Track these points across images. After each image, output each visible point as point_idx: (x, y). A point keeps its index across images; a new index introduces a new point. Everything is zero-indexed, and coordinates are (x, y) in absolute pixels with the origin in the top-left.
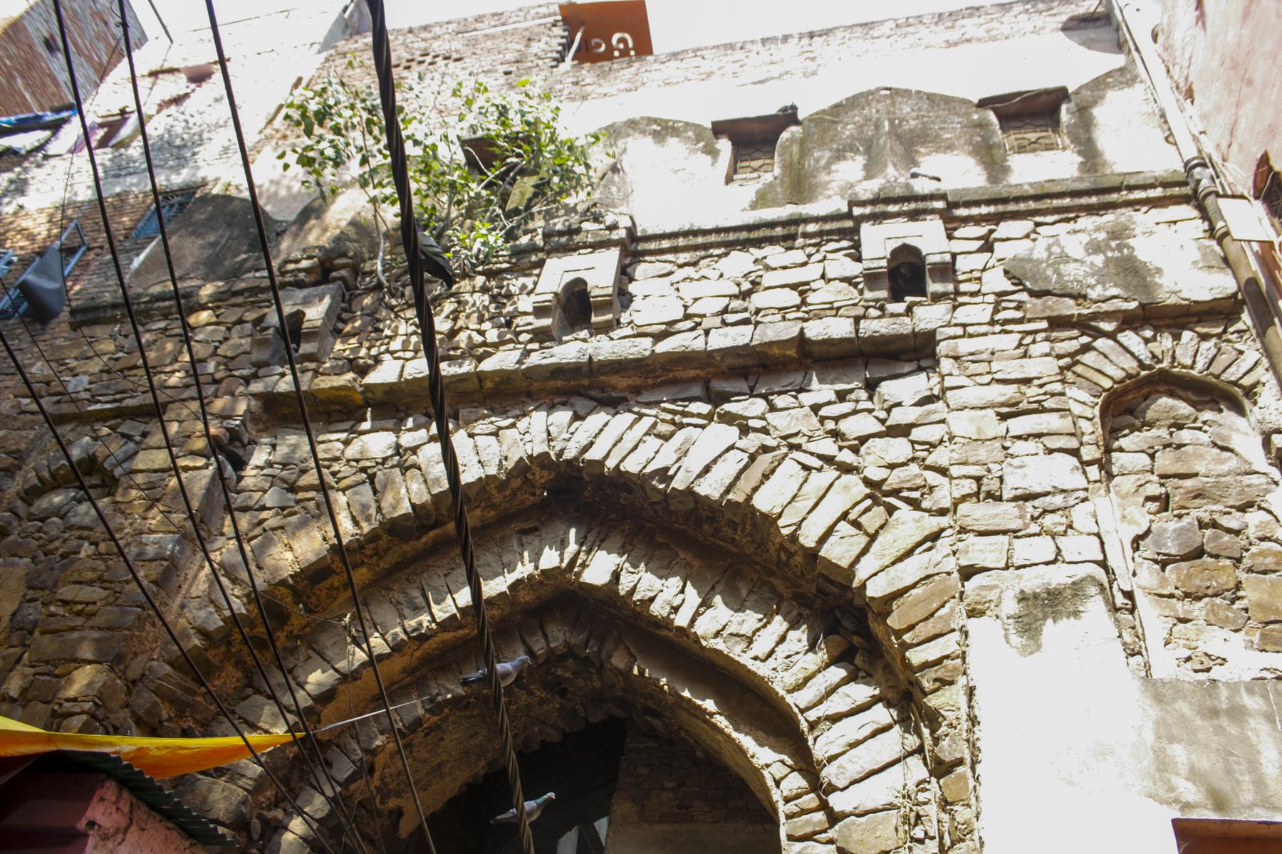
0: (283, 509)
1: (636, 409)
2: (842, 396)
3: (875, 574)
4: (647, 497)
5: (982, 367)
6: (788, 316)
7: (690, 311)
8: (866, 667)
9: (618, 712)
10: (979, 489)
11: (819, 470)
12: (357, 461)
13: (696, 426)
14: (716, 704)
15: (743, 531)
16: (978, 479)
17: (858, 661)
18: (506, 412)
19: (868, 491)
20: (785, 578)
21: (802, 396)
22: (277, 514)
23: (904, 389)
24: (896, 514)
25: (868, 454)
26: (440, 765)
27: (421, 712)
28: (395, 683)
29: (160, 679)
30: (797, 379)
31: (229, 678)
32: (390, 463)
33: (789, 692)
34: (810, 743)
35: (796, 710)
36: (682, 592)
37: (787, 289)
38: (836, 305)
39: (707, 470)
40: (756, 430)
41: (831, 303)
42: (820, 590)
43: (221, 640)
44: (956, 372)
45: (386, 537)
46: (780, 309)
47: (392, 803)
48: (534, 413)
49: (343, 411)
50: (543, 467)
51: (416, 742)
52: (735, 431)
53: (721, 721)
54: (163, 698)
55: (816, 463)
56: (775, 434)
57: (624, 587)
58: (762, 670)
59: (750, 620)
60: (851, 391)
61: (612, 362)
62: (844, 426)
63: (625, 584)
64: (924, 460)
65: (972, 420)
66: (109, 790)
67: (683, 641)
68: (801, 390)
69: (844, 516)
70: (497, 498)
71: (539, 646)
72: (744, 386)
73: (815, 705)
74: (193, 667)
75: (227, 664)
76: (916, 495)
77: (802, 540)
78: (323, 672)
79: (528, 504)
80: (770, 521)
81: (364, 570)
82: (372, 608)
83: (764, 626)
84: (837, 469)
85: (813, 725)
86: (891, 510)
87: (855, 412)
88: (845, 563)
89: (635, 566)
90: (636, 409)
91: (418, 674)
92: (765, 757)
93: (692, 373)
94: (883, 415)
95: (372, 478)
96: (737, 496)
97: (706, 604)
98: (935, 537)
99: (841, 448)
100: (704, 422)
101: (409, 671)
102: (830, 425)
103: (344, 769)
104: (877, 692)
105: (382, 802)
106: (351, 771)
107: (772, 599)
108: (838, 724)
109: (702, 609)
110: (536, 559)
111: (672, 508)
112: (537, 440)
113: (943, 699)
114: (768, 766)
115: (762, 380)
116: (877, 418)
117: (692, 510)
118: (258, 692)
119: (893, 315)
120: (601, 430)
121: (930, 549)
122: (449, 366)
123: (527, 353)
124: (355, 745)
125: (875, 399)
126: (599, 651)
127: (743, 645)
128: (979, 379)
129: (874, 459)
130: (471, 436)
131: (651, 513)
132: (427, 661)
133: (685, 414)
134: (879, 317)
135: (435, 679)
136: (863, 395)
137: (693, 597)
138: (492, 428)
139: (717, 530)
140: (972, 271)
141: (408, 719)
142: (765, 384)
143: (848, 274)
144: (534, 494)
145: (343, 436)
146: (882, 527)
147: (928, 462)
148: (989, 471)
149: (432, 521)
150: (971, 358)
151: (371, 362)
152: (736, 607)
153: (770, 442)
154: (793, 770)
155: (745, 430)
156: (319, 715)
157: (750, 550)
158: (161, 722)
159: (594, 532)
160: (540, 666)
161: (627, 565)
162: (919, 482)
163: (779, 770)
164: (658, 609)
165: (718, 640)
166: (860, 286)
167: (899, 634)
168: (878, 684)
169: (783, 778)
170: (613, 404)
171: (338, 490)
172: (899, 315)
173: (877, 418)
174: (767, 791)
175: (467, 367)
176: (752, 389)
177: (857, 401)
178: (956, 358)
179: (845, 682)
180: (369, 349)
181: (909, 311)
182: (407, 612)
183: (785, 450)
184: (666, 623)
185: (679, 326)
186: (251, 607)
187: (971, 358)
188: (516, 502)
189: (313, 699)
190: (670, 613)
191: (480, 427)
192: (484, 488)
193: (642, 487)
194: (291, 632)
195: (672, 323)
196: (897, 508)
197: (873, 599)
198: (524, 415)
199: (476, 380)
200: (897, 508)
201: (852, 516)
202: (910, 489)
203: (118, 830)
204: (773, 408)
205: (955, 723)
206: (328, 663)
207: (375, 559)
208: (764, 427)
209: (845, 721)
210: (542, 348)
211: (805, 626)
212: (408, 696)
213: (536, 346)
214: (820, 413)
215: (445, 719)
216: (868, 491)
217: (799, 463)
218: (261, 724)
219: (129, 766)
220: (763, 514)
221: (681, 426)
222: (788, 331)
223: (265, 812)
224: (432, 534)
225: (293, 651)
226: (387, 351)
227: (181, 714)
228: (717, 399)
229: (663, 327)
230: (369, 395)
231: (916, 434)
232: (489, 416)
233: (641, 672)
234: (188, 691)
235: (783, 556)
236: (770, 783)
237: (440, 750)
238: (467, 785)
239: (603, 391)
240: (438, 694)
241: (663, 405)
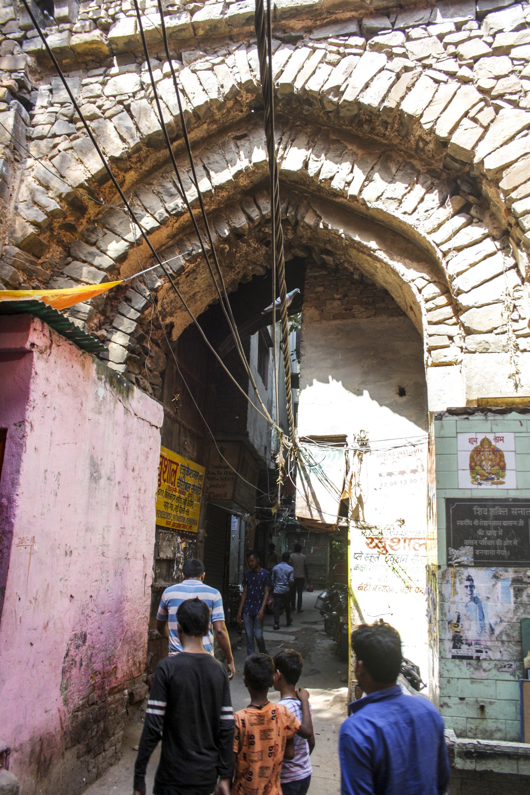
0: (69, 135)
1: (310, 44)
2: (459, 27)
3: (490, 154)
4: (323, 107)
8: (479, 216)
9: (301, 254)
11: (446, 83)
12: (115, 96)
13: (355, 54)
14: (377, 243)
15: (392, 128)
17: (473, 212)
18: (216, 52)
19: (481, 96)
20: (421, 160)
21: (430, 28)
22: (66, 139)
24: (501, 112)
25: (481, 69)
26: (195, 295)
27: (183, 262)
28: (162, 246)
29: (14, 256)
30: (425, 15)
31: (55, 253)
32: (139, 96)
33: (429, 233)
34: (444, 265)
35: (434, 245)
36: (352, 172)
39: (367, 86)
40: (398, 55)
42: (445, 167)
43: (47, 228)
45: (145, 149)
47: (168, 320)
48: (237, 52)
49: (92, 60)
50: (248, 91)
51: (180, 281)
52: (384, 57)
53: (381, 255)
54: (18, 269)
55: (444, 77)
56: (412, 57)
57: (312, 172)
58: (409, 220)
59: (398, 188)
60: (466, 22)
61: (292, 9)
62: (462, 49)
64: (520, 72)
66: (37, 324)
67: (354, 204)
68: (429, 24)
69: (466, 114)
70: (218, 115)
71: (255, 214)
72: (386, 22)
73: (446, 241)
74: (32, 246)
75: (52, 243)
76: (515, 97)
77: (437, 132)
78: (117, 242)
79: (238, 118)
80: (415, 120)
81: (132, 173)
82: (141, 198)
83: (409, 192)
84: (458, 82)
85: (445, 254)
86: (498, 109)
87: (470, 38)
88: (468, 147)
89: (318, 157)
90: (310, 44)
91: (177, 238)
92: (412, 275)
93: (349, 15)
94: (490, 40)
95: (128, 108)
96: (391, 103)
97: (369, 179)
99: (460, 66)
100: (360, 51)
101: (172, 237)
102: (452, 49)
103: (141, 303)
104: (486, 231)
105: (163, 320)
106: (144, 303)
107: (413, 174)
108: (461, 252)
109: (366, 183)
110: (249, 155)
111: (341, 115)
114: (413, 281)
115: (400, 17)
116: (485, 42)
117: (356, 115)
118: (76, 259)
120: (287, 61)
121: (526, 135)
122: (171, 19)
124: (143, 287)
125: (483, 27)
126: (296, 214)
127: (397, 204)
129: (486, 71)
130: (194, 72)
131: (325, 119)
132: (182, 229)
133: (346, 46)
135: (189, 240)
137: (359, 175)
138: (208, 65)
139: (373, 129)
141: (176, 267)
142: (403, 20)
144: (242, 111)
145: (101, 79)
146: (492, 121)
147: (523, 74)
149: (174, 135)
151: (110, 21)
152: (390, 180)
153: (410, 63)
154: (430, 282)
155: (391, 56)
156: (119, 270)
157: (396, 141)
158: (20, 284)
159: (287, 135)
160: (256, 227)
161: (313, 156)
162: (518, 88)
163: (421, 283)
164: (337, 184)
165: (379, 202)
167: (507, 193)
168: (487, 226)
169: (423, 287)
171: (105, 118)
173: (485, 42)
174: (414, 295)
175: (184, 19)
176: (393, 24)
177: (471, 30)
180: (107, 10)
182: (166, 198)
183: (420, 69)
184: (341, 194)
186: (63, 204)
188: (230, 118)
189: (114, 260)
190: (345, 186)
191: (199, 65)
192: (209, 109)
193: (321, 101)
194: (89, 219)
196: (502, 108)
197: (489, 170)
198: (230, 54)
199: (191, 30)
200: (502, 108)
201: (471, 115)
202: (511, 94)
203: (46, 347)
204: (409, 39)
206: (120, 236)
207: (139, 164)
208: (404, 53)
209: (466, 250)
211: (436, 191)
212: (173, 253)
215: (197, 266)
216: (481, 96)
217: (432, 78)
218: (83, 279)
219: (49, 308)
220: (409, 115)
221: (344, 55)
223: (95, 332)
225: (93, 231)
226: (121, 11)
227: (30, 278)
228: (368, 33)
230: (114, 46)
231: (514, 53)
232: (204, 56)
233: (326, 227)
234: (32, 262)
235: (421, 145)
236: (415, 291)
237: (194, 286)
238: (209, 306)
239: (284, 32)
240: (193, 250)
241: (329, 40)
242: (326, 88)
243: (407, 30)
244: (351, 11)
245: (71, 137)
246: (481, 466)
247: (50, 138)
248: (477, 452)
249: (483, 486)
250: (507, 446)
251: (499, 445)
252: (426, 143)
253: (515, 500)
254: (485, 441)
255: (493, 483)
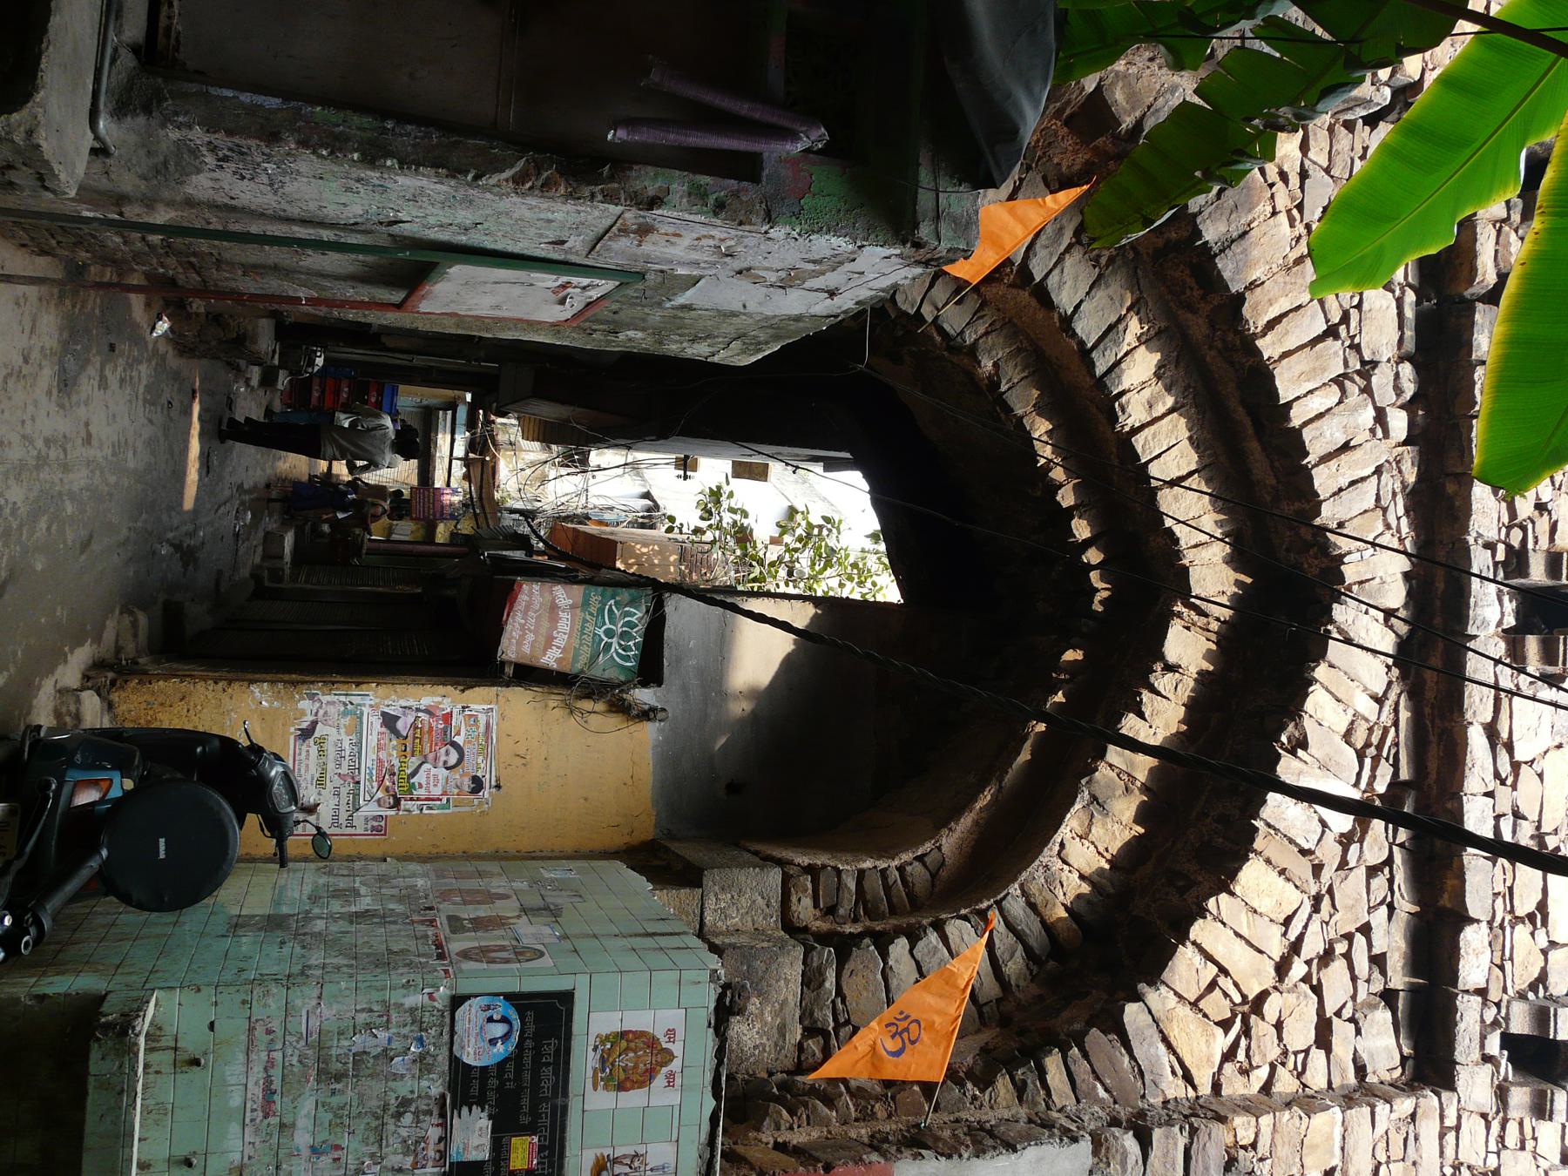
0: (1300, 207)
2: (1378, 961)
5: (1396, 1151)
6: (1500, 900)
7: (1524, 768)
10: (1244, 1148)
11: (1285, 934)
12: (1359, 306)
13: (1359, 775)
16: (1254, 1145)
17: (1051, 964)
23: (1382, 1044)
24: (1219, 1031)
33: (1022, 886)
37: (1540, 897)
38: (1508, 965)
41: (1511, 959)
44: (1394, 1116)
46: (1511, 889)
55: (1293, 934)
60: (1383, 972)
62: (1339, 965)
63: (1163, 682)
64: (1283, 1064)
65: (1330, 1137)
69: (1223, 971)
76: (1241, 1055)
81: (1205, 330)
85: (982, 914)
86: (1225, 1025)
87: (1354, 979)
92: (951, 841)
93: (1432, 766)
94: (1347, 1013)
95: (1331, 332)
98: (1188, 1078)
102: (1341, 948)
112: (1362, 568)
113: (1002, 1092)
116: (1344, 1006)
119: (1483, 1038)
121: (1174, 1073)
123: (1490, 546)
124: (981, 330)
128: (1382, 1145)
130: (1378, 471)
133: (1376, 760)
134: (1483, 1021)
136: (1378, 986)
140: (1535, 1139)
143: (1552, 979)
146: (1205, 1016)
148: (1261, 1160)
150: (1411, 1137)
166: (1531, 996)
170: (1406, 658)
172: (1482, 1046)
173: (1344, 1006)
178: (1413, 1116)
179: (1028, 950)
181: (1487, 1059)
185: (1503, 757)
187: (1411, 1137)
195: (1509, 747)
201: (1222, 981)
205: (977, 1103)
207: (1219, 344)
210: (1496, 564)
213: (1501, 556)
214: (1358, 935)
221: (1361, 756)
222: (1476, 903)
224: (1248, 422)
229: (1505, 735)
231: (1318, 1056)
242: (1307, 723)
243: (1386, 870)
244: (1438, 773)
245: (1295, 212)
246: (627, 1049)
247: (1302, 164)
248: (651, 1042)
249: (591, 1054)
250: (660, 1095)
251: (660, 1081)
252: (1182, 891)
253: (565, 1109)
254: (669, 1056)
255: (595, 1070)
